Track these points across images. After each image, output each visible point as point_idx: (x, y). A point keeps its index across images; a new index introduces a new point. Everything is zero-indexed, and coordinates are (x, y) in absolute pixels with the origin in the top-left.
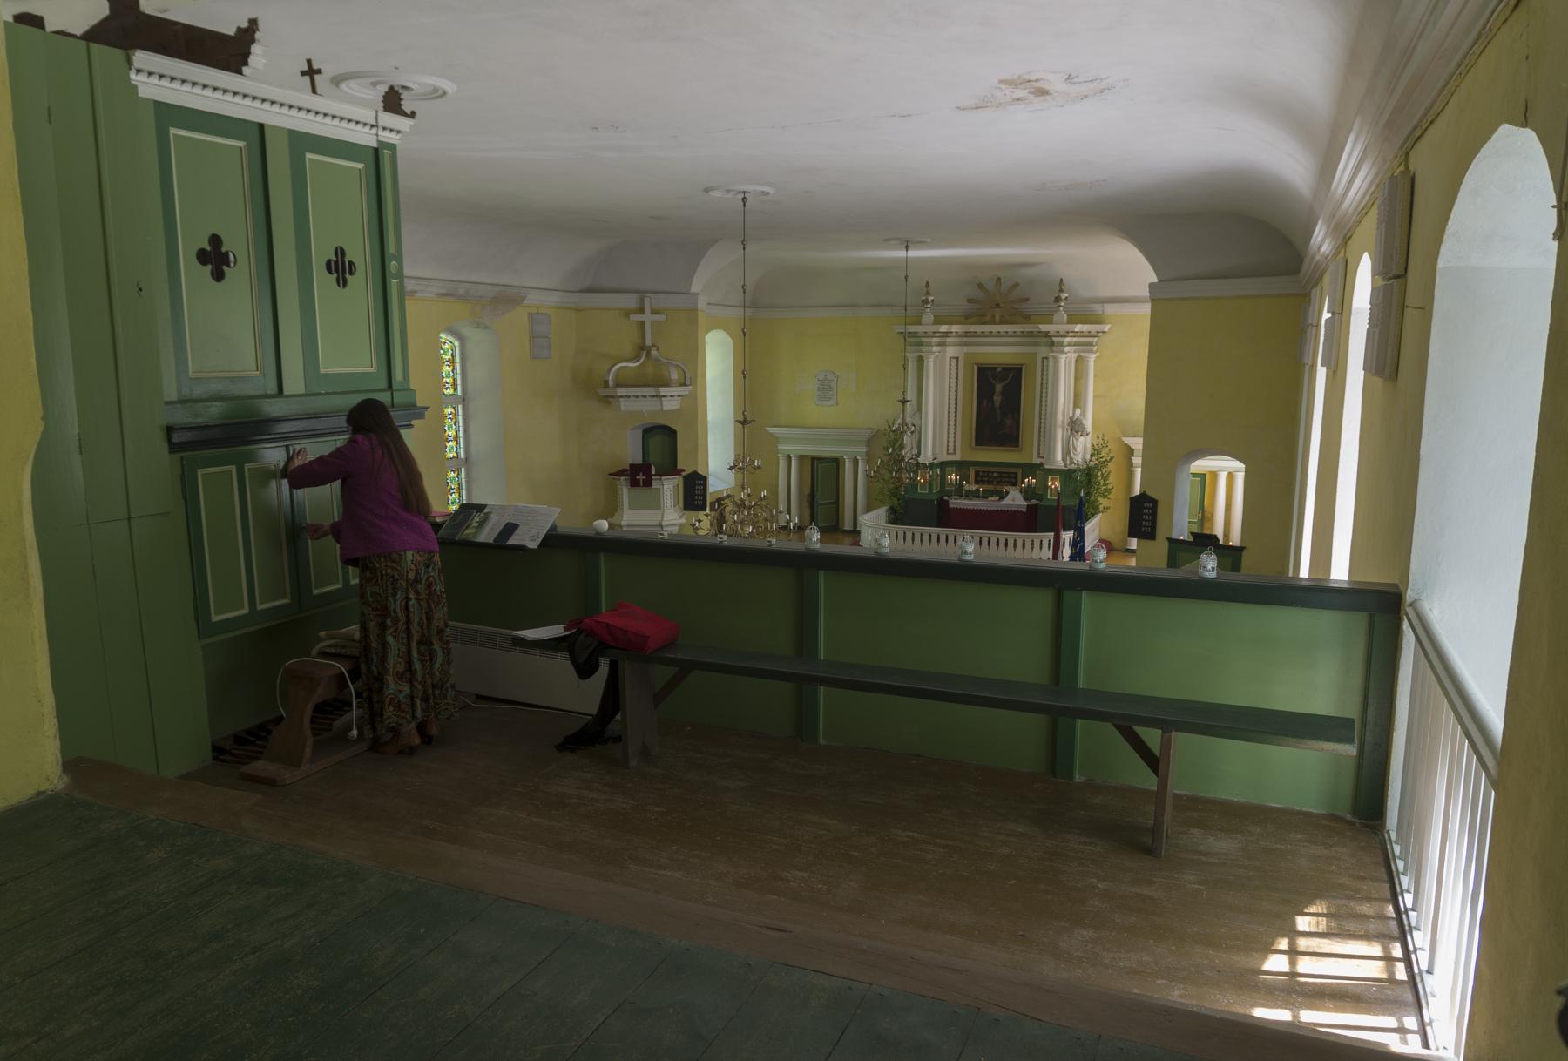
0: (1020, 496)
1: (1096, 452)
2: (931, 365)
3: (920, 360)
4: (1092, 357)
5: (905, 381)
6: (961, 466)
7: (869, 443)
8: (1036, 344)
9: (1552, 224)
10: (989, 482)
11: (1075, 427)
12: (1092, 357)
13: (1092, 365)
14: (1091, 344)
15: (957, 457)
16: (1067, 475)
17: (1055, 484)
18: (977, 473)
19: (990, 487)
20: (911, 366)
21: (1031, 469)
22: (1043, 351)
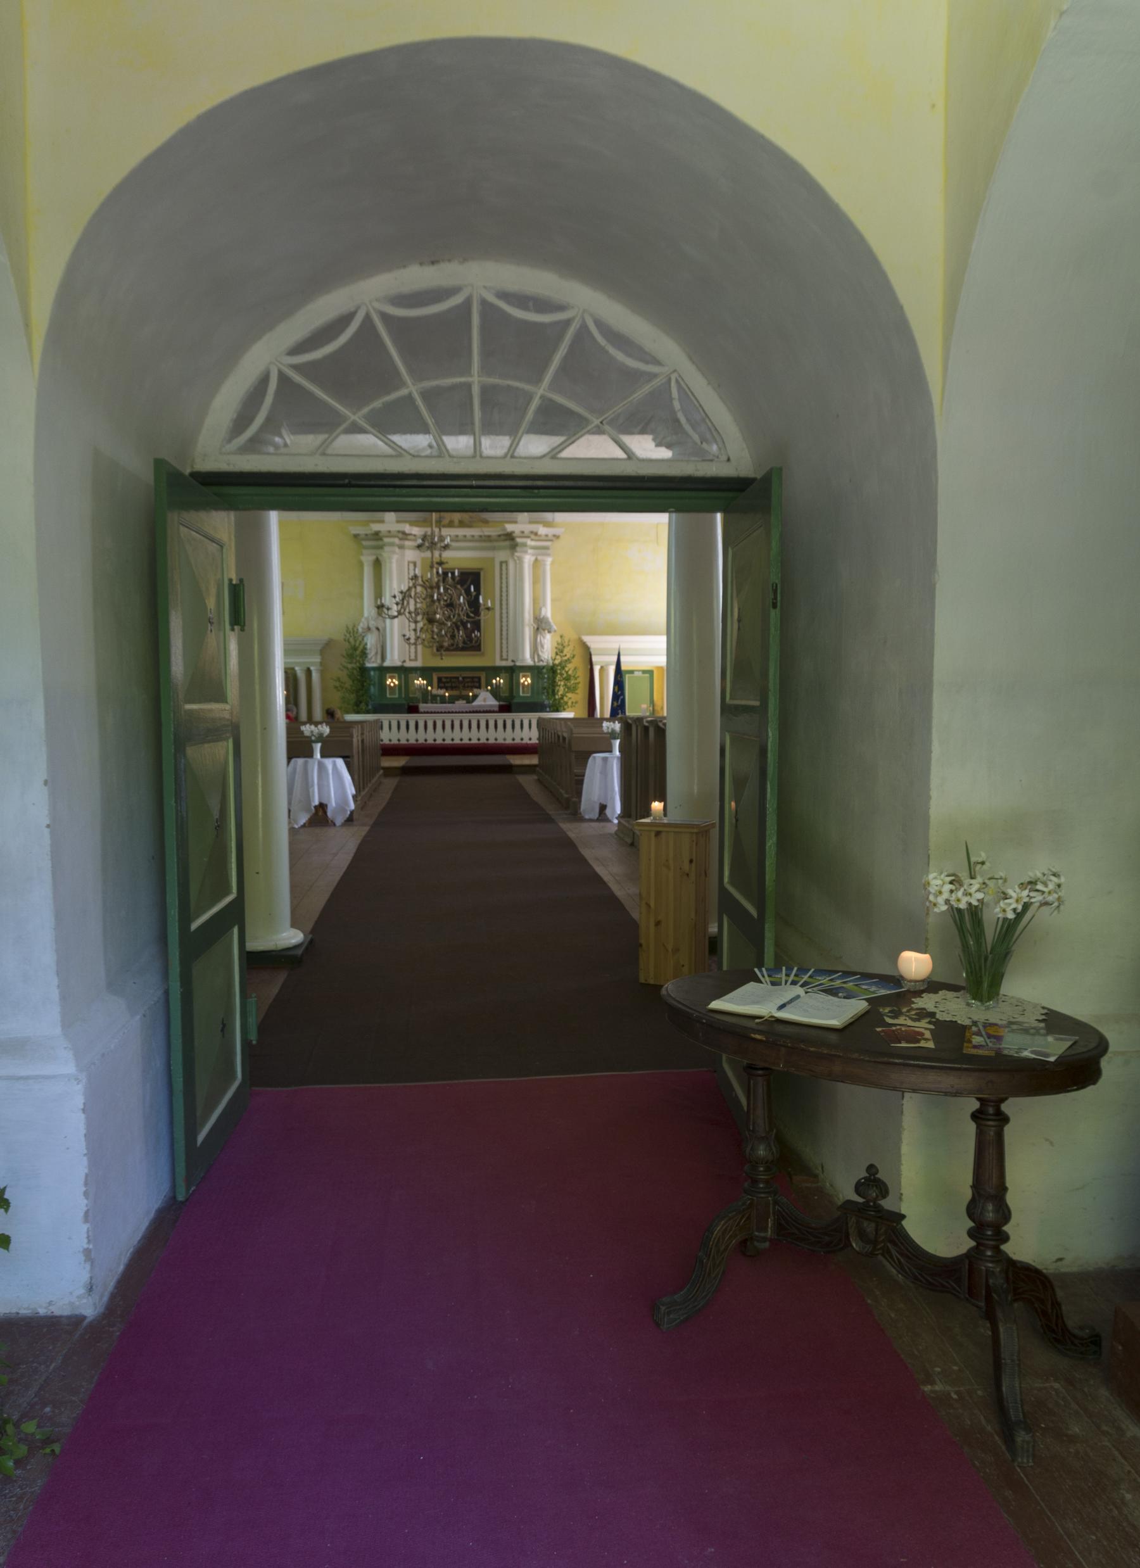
0: (489, 695)
1: (559, 651)
2: (394, 566)
3: (378, 564)
4: (549, 560)
5: (362, 587)
6: (425, 672)
7: (322, 652)
8: (494, 549)
9: (971, 1183)
10: (452, 688)
11: (541, 625)
12: (549, 560)
13: (548, 568)
14: (547, 548)
15: (418, 664)
16: (535, 671)
17: (526, 680)
18: (440, 680)
19: (455, 693)
20: (368, 571)
21: (496, 671)
22: (501, 555)
